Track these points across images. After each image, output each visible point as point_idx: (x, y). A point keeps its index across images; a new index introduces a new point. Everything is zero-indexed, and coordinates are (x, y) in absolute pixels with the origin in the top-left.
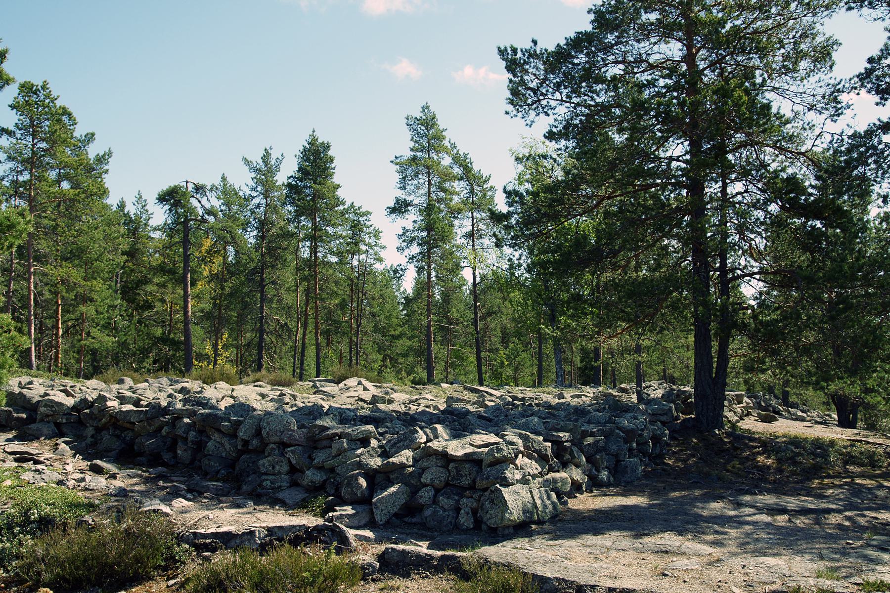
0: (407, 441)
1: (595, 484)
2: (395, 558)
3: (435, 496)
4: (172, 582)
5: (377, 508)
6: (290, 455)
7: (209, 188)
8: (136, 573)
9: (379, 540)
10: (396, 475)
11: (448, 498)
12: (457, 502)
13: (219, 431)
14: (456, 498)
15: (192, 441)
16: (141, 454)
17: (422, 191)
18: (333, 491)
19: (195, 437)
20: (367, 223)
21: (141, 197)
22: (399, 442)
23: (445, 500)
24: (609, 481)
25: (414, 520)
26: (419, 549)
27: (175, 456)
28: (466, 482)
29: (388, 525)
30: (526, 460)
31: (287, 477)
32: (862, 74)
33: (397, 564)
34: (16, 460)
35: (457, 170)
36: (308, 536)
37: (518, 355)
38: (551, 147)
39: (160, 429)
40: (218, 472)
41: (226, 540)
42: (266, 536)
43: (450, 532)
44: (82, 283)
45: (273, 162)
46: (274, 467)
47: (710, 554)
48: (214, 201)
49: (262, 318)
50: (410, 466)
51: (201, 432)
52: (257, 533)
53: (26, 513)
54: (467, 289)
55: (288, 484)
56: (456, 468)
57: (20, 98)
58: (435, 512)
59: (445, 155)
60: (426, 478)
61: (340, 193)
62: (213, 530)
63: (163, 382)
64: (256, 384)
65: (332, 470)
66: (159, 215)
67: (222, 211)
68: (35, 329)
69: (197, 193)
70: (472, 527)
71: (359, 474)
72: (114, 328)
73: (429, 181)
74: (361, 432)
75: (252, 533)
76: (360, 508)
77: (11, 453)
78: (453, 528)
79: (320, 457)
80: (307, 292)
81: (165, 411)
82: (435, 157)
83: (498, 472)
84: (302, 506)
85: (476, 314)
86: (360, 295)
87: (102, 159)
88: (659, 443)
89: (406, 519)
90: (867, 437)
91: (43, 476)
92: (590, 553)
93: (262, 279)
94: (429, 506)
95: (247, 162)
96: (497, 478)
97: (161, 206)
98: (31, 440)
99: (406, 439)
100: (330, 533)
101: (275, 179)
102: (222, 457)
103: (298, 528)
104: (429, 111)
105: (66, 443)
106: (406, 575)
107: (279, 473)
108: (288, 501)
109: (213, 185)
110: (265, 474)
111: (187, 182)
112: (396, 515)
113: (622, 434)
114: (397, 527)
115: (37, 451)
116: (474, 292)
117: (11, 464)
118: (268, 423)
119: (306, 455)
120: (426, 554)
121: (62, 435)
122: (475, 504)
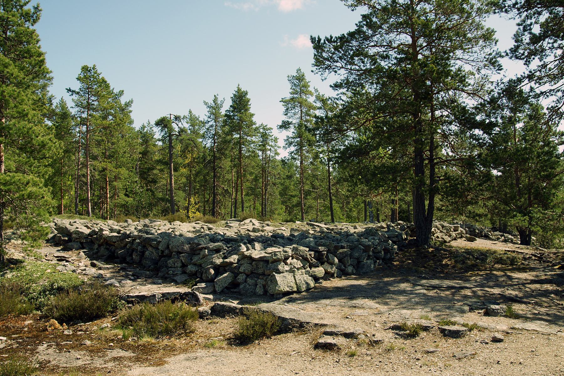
0: (236, 250)
1: (343, 273)
3: (246, 278)
4: (114, 318)
5: (217, 284)
6: (182, 258)
7: (182, 117)
8: (97, 314)
9: (215, 300)
10: (228, 268)
12: (256, 281)
13: (151, 246)
14: (256, 279)
15: (140, 251)
16: (118, 258)
17: (297, 116)
18: (200, 276)
20: (270, 134)
21: (149, 123)
22: (232, 251)
23: (250, 280)
24: (353, 272)
25: (235, 290)
26: (231, 304)
27: (132, 259)
28: (260, 271)
29: (222, 292)
30: (295, 260)
31: (180, 269)
32: (513, 49)
33: (219, 311)
34: (58, 260)
35: (319, 104)
36: (182, 297)
38: (333, 94)
39: (126, 245)
40: (150, 266)
41: (142, 299)
42: (161, 297)
43: (251, 296)
44: (114, 170)
45: (219, 102)
46: (174, 264)
47: (377, 308)
48: (186, 125)
49: (214, 186)
50: (235, 263)
51: (144, 247)
52: (157, 296)
53: (52, 285)
56: (256, 264)
57: (82, 74)
58: (245, 286)
59: (310, 96)
60: (242, 269)
61: (254, 119)
62: (137, 294)
63: (146, 222)
65: (200, 265)
66: (158, 134)
67: (190, 129)
69: (176, 120)
71: (211, 267)
72: (135, 193)
73: (301, 110)
75: (154, 296)
76: (209, 284)
77: (56, 257)
79: (195, 259)
80: (237, 172)
81: (128, 236)
82: (304, 97)
84: (185, 283)
86: (267, 173)
87: (128, 104)
89: (231, 290)
90: (522, 249)
91: (67, 268)
92: (317, 307)
94: (243, 283)
95: (206, 103)
97: (157, 128)
98: (68, 251)
99: (235, 249)
100: (191, 296)
101: (220, 111)
102: (153, 259)
104: (300, 72)
105: (84, 252)
106: (223, 317)
107: (177, 267)
108: (178, 281)
109: (184, 116)
110: (171, 267)
111: (170, 115)
112: (226, 288)
113: (362, 247)
115: (69, 256)
117: (55, 261)
118: (172, 242)
119: (190, 258)
120: (234, 307)
121: (83, 248)
122: (264, 283)
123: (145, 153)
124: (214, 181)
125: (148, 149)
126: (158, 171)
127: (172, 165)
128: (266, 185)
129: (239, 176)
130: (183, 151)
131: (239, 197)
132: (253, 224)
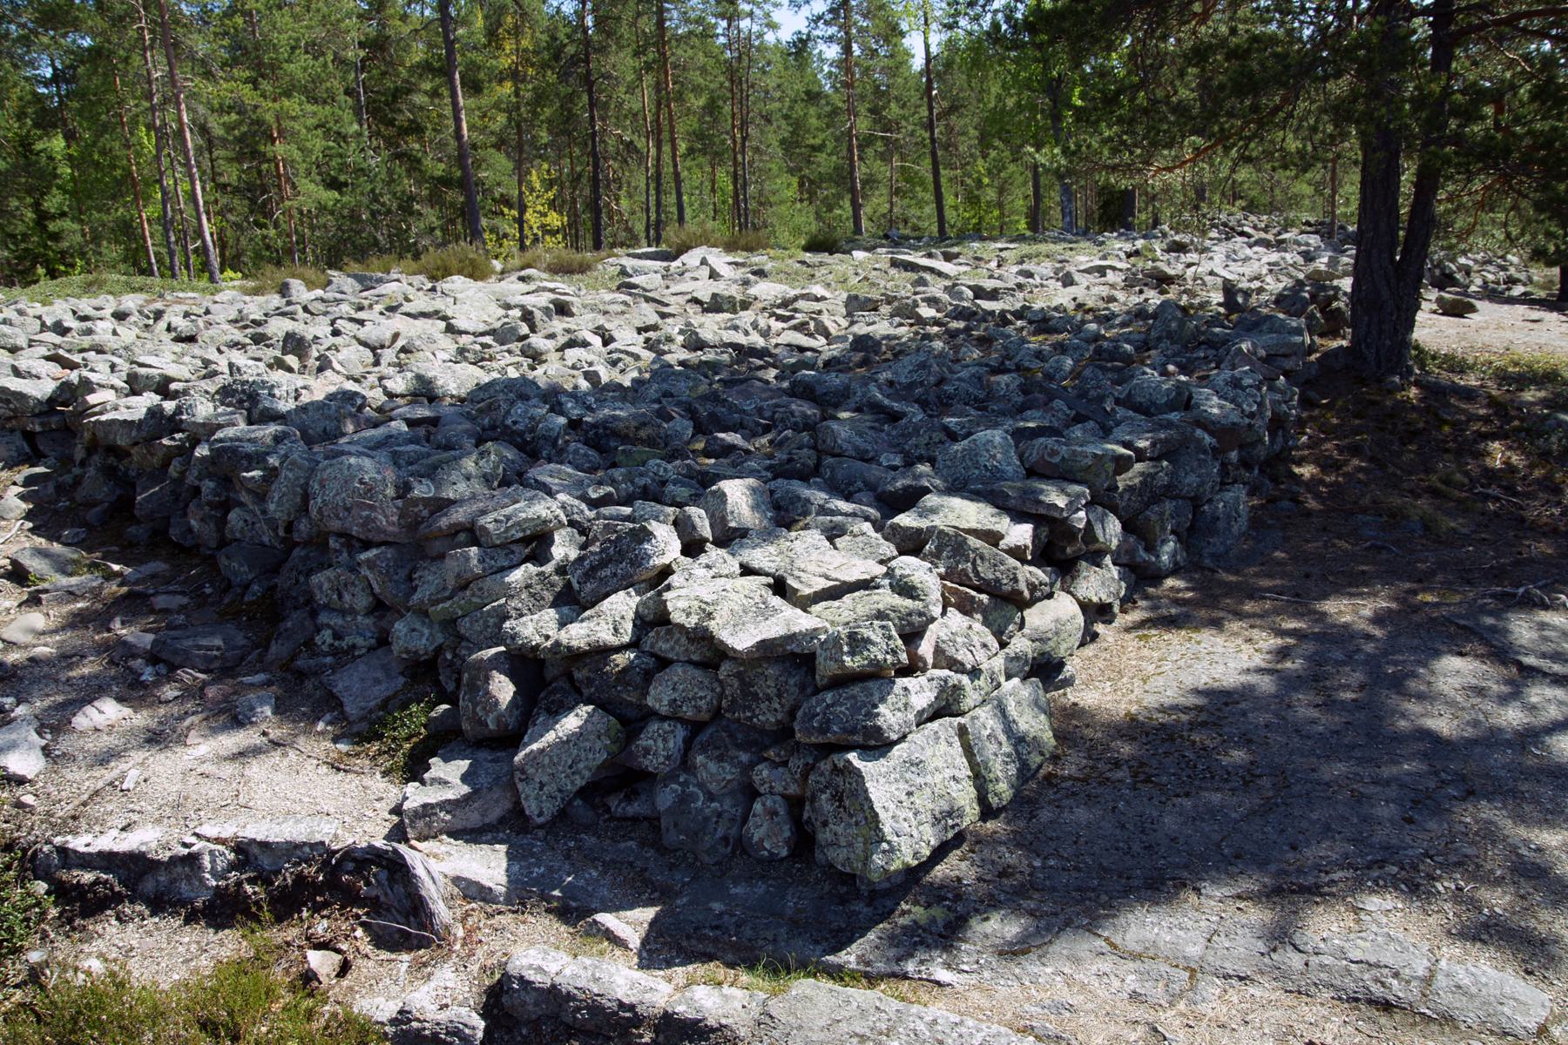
2: (531, 1008)
5: (527, 780)
11: (720, 759)
14: (744, 757)
19: (215, 493)
22: (603, 564)
23: (712, 766)
28: (768, 716)
31: (369, 621)
37: (1004, 168)
39: (166, 464)
40: (247, 587)
42: (232, 866)
46: (340, 596)
52: (206, 861)
54: (918, 63)
55: (373, 641)
56: (739, 675)
58: (684, 799)
64: (523, 273)
65: (450, 623)
68: (203, 189)
70: (784, 853)
71: (495, 663)
74: (518, 524)
75: (193, 860)
78: (733, 852)
80: (658, 87)
83: (855, 709)
85: (931, 109)
88: (1283, 428)
93: (589, 72)
94: (672, 777)
96: (853, 731)
99: (621, 555)
100: (384, 875)
102: (263, 545)
103: (307, 849)
107: (352, 611)
113: (1208, 439)
114: (586, 828)
116: (927, 70)
119: (403, 573)
123: (377, 46)
124: (592, 118)
125: (389, 32)
126: (426, 99)
127: (457, 76)
128: (744, 125)
129: (662, 99)
130: (492, 33)
131: (666, 157)
132: (714, 275)
